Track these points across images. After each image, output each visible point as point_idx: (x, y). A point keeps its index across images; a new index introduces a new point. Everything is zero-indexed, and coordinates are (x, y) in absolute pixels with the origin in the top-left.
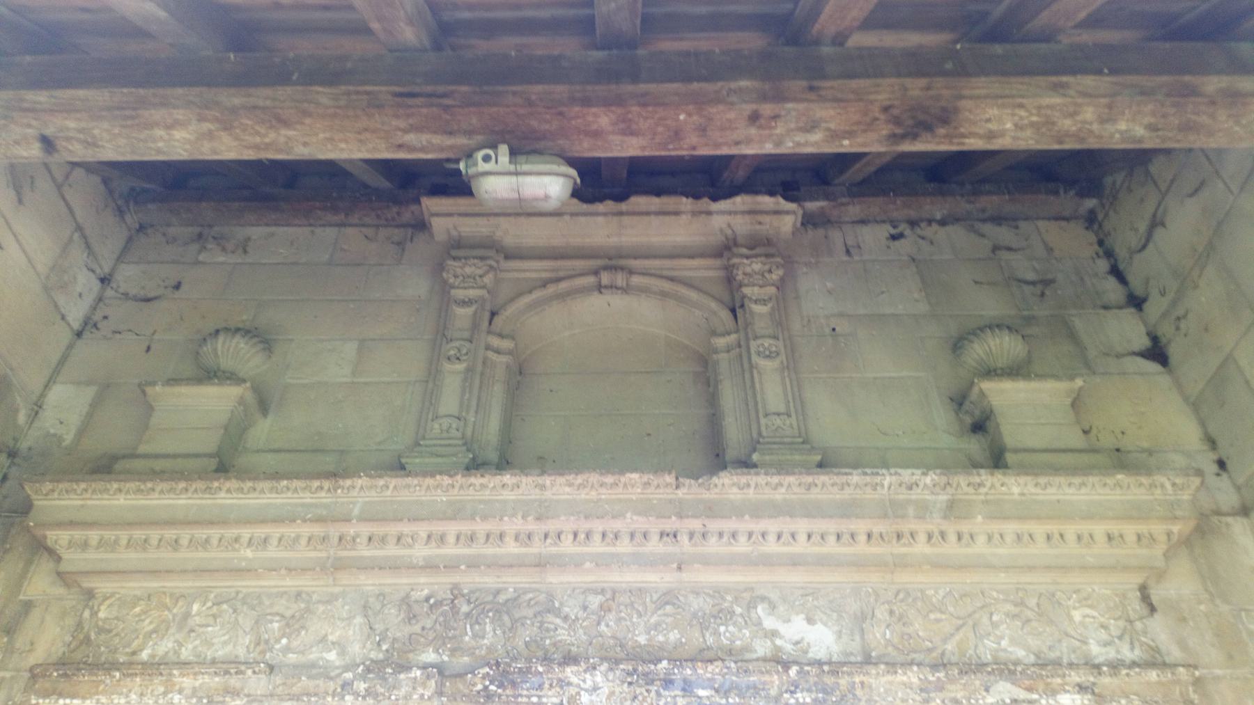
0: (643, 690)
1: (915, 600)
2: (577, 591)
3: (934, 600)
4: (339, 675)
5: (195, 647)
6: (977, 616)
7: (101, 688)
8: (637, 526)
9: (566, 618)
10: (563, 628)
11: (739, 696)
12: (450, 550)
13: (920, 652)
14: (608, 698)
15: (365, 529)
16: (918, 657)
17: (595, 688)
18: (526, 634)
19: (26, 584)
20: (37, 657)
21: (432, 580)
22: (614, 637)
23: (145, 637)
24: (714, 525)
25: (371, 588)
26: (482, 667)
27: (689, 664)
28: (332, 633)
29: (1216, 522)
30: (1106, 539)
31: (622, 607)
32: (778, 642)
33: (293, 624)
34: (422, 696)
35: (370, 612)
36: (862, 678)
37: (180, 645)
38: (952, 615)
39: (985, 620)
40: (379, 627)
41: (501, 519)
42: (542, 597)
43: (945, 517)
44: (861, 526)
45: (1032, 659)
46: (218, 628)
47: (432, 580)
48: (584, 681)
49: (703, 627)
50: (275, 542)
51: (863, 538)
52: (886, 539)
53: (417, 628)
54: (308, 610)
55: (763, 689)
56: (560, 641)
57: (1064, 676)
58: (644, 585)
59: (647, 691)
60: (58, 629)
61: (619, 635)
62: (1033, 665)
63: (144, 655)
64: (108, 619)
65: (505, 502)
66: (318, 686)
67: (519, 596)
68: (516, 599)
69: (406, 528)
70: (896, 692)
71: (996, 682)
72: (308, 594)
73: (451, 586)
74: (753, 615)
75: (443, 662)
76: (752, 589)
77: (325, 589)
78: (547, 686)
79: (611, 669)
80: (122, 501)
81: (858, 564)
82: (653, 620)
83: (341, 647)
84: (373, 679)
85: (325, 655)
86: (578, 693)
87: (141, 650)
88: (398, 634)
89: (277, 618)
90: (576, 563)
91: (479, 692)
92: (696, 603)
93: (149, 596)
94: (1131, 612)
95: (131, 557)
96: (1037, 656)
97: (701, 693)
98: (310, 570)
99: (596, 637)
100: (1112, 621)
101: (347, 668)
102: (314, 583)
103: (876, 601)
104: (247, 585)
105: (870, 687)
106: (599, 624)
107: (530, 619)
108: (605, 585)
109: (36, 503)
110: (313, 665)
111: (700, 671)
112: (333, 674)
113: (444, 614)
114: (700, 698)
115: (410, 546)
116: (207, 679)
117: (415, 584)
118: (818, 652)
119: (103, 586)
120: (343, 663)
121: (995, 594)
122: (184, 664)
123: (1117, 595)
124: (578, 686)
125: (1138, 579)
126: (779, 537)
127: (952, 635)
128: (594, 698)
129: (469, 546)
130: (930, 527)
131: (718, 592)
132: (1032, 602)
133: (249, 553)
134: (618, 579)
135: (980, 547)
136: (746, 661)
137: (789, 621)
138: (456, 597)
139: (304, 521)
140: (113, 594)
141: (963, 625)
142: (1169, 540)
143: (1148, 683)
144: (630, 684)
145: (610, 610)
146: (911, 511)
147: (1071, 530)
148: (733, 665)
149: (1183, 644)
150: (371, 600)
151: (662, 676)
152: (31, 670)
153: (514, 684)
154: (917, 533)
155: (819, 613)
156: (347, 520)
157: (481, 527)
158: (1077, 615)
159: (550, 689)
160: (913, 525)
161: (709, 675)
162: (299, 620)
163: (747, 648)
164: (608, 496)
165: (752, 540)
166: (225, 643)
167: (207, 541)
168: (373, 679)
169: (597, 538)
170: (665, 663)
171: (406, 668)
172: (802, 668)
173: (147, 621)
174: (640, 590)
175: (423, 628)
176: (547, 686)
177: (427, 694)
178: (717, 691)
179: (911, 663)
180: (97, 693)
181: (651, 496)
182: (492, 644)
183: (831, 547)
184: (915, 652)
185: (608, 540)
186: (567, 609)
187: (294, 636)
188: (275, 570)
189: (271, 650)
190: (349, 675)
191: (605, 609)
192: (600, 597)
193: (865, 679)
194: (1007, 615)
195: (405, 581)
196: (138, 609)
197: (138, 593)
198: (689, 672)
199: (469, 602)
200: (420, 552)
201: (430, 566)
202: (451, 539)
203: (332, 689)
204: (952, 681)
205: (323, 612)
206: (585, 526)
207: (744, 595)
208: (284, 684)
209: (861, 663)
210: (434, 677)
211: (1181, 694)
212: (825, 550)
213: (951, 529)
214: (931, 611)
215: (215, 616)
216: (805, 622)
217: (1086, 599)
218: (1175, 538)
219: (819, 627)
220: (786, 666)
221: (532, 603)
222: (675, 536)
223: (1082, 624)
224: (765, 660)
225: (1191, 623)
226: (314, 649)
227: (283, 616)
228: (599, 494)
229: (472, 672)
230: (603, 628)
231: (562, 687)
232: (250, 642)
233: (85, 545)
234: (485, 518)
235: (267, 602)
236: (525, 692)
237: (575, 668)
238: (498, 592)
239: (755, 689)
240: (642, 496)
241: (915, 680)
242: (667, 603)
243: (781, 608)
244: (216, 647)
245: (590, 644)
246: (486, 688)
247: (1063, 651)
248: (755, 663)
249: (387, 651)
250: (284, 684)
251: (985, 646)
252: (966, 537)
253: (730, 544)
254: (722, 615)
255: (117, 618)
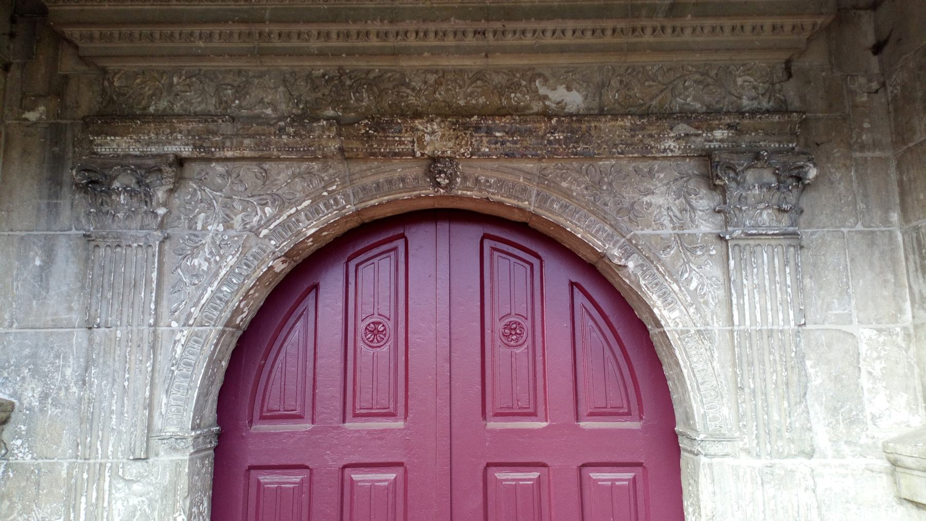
0: (462, 133)
1: (638, 73)
2: (420, 71)
3: (650, 73)
4: (276, 123)
5: (182, 105)
6: (676, 83)
7: (131, 130)
8: (458, 27)
9: (413, 89)
10: (412, 96)
11: (520, 136)
12: (334, 43)
13: (635, 107)
14: (441, 138)
15: (276, 28)
16: (633, 109)
17: (433, 132)
18: (388, 100)
19: (59, 64)
20: (83, 111)
21: (325, 63)
22: (443, 101)
23: (148, 98)
24: (510, 26)
25: (285, 68)
26: (363, 120)
27: (491, 118)
28: (266, 97)
29: (853, 14)
30: (771, 29)
31: (449, 82)
32: (547, 103)
33: (241, 91)
34: (329, 136)
35: (288, 84)
36: (596, 124)
37: (173, 104)
38: (660, 82)
39: (681, 86)
40: (295, 93)
41: (366, 22)
42: (398, 75)
43: (666, 17)
44: (609, 24)
45: (704, 109)
46: (193, 93)
47: (325, 63)
48: (427, 128)
49: (501, 95)
50: (217, 36)
51: (609, 32)
52: (625, 32)
53: (320, 95)
54: (247, 82)
55: (535, 132)
56: (411, 104)
57: (721, 119)
58: (464, 67)
59: (465, 133)
60: (91, 93)
61: (448, 100)
62: (703, 113)
63: (152, 109)
64: (121, 87)
65: (367, 9)
66: (264, 130)
67: (383, 74)
68: (380, 76)
69: (303, 28)
70: (616, 132)
71: (678, 124)
72: (246, 72)
73: (337, 68)
74: (533, 86)
75: (339, 116)
76: (534, 69)
77: (255, 68)
78: (404, 131)
79: (442, 121)
80: (107, 7)
81: (604, 50)
82: (468, 91)
83: (271, 104)
84: (297, 126)
85: (264, 111)
86: (423, 135)
87: (149, 107)
88: (308, 98)
89: (229, 87)
90: (418, 52)
91: (363, 134)
92: (497, 79)
93: (143, 72)
94: (775, 78)
95: (125, 45)
96: (708, 107)
97: (498, 134)
98: (244, 56)
99: (433, 101)
100: (761, 84)
101: (280, 119)
102: (248, 64)
103: (613, 74)
104: (206, 65)
105: (600, 129)
106: (435, 93)
107: (391, 90)
108: (437, 67)
109: (50, 8)
110: (258, 117)
111: (497, 122)
112: (272, 122)
113: (335, 86)
114: (497, 137)
115: (307, 41)
116: (195, 125)
117: (314, 66)
118: (571, 108)
119: (112, 65)
120: (276, 116)
121: (690, 68)
122: (178, 116)
123: (769, 67)
124: (423, 131)
125: (785, 56)
126: (554, 33)
127: (657, 95)
128: (432, 137)
129: (347, 41)
130: (655, 23)
131: (512, 71)
132: (713, 73)
133: (201, 44)
134: (447, 63)
135: (687, 36)
136: (526, 115)
137: (556, 89)
138: (342, 75)
139: (234, 22)
140: (119, 71)
141: (667, 88)
142: (813, 29)
143: (772, 123)
144: (454, 130)
145: (441, 84)
146: (644, 12)
147: (749, 23)
148: (517, 118)
149: (802, 98)
150: (288, 76)
151: (474, 125)
152: (83, 119)
153: (384, 130)
154: (646, 27)
155: (576, 84)
156: (262, 22)
157: (353, 28)
158: (739, 81)
159: (406, 133)
160: (644, 22)
161: (502, 124)
162: (243, 88)
163: (527, 107)
164: (438, 5)
165: (535, 36)
166: (199, 102)
167: (172, 35)
168: (297, 126)
169: (431, 35)
170: (476, 117)
171: (317, 119)
172: (559, 119)
173: (147, 89)
174: (461, 70)
175: (324, 95)
176: (404, 131)
177: (332, 135)
178: (507, 133)
179: (627, 115)
180: (129, 133)
181: (468, 5)
182: (368, 105)
183: (588, 39)
184: (632, 106)
185: (439, 37)
186: (414, 84)
187: (242, 99)
188: (221, 55)
189: (230, 107)
190: (282, 124)
191: (438, 83)
192: (435, 75)
193: (597, 124)
194: (695, 81)
195: (307, 64)
196: (138, 81)
197: (136, 70)
198: (490, 122)
199: (350, 78)
200: (315, 44)
201: (322, 54)
202: (334, 36)
203: (273, 131)
204: (651, 124)
205: (258, 84)
206: (424, 27)
207: (528, 73)
208: (243, 128)
209: (597, 115)
210: (334, 125)
211: (791, 129)
212: (583, 41)
213: (669, 24)
214: (646, 80)
215: (189, 86)
216: (565, 90)
217: (749, 70)
218: (817, 28)
219: (574, 92)
220: (550, 118)
221: (391, 79)
222: (484, 34)
223: (742, 87)
224: (537, 114)
225: (813, 84)
226: (257, 107)
227: (232, 86)
228: (432, 3)
229: (358, 123)
230: (437, 95)
231: (413, 132)
232: (216, 102)
233: (91, 38)
234: (355, 21)
235: (221, 77)
236: (391, 135)
237: (420, 121)
238: (368, 72)
239: (530, 132)
240: (461, 5)
241: (628, 124)
242: (478, 79)
243: (551, 81)
244: (194, 105)
245: (430, 105)
246: (367, 132)
247: (725, 104)
248: (531, 117)
249: (303, 108)
250: (243, 128)
251: (676, 102)
252: (678, 30)
253: (521, 39)
254: (514, 86)
255: (126, 86)
